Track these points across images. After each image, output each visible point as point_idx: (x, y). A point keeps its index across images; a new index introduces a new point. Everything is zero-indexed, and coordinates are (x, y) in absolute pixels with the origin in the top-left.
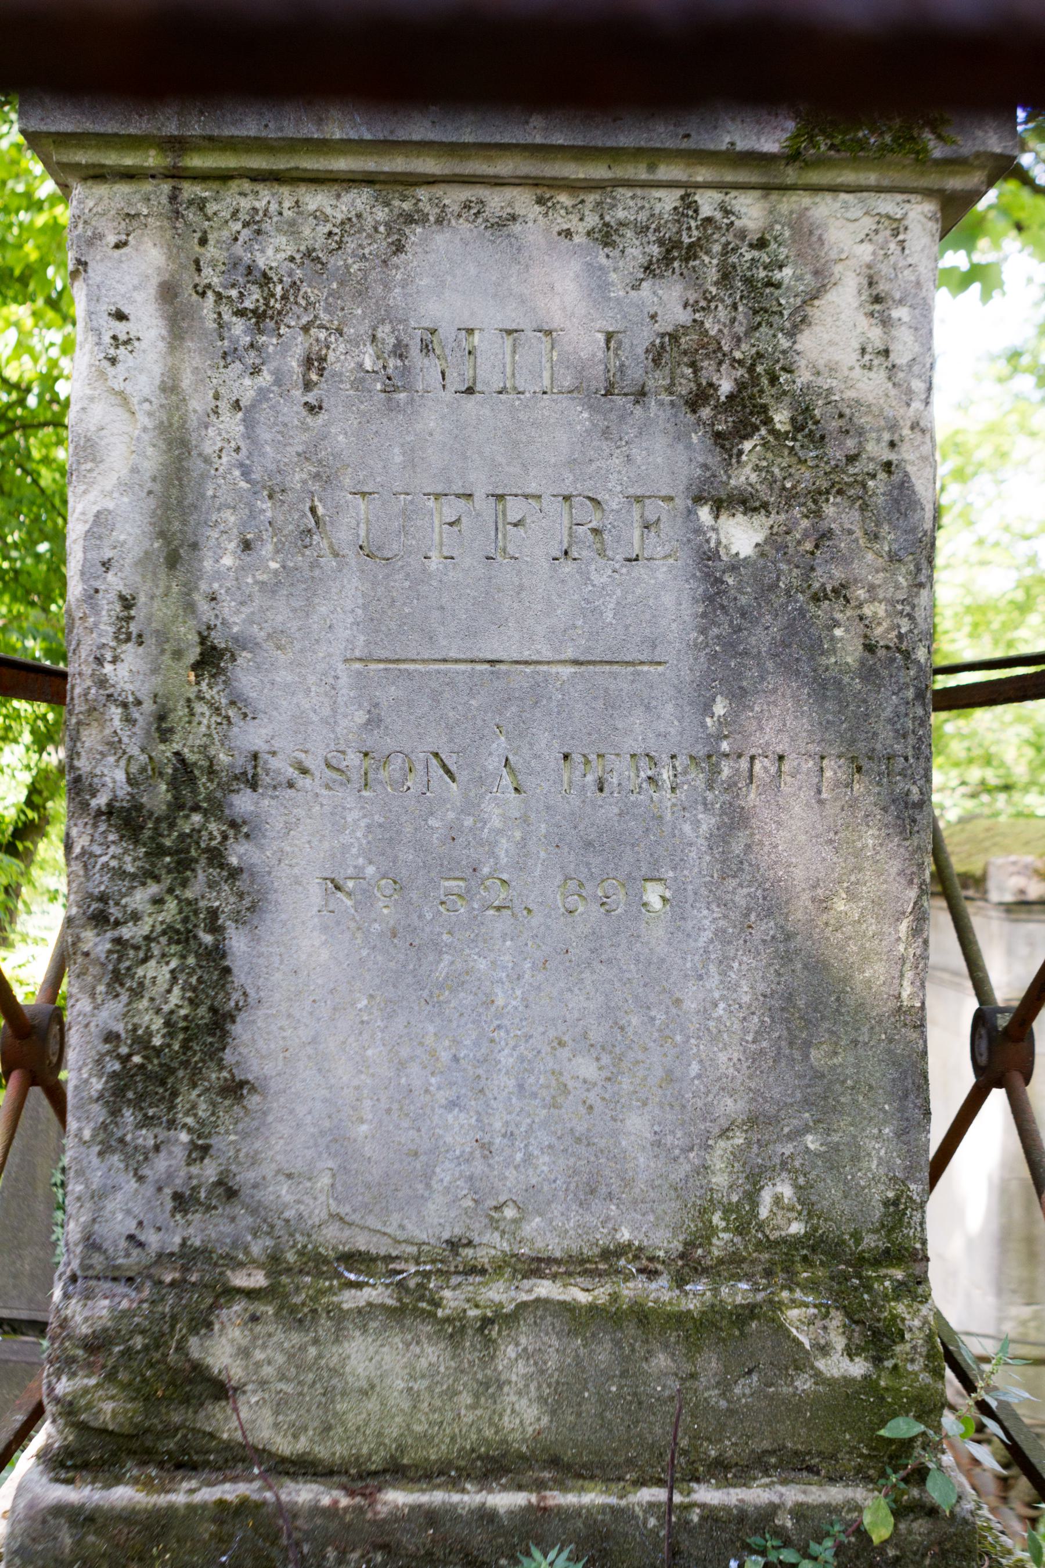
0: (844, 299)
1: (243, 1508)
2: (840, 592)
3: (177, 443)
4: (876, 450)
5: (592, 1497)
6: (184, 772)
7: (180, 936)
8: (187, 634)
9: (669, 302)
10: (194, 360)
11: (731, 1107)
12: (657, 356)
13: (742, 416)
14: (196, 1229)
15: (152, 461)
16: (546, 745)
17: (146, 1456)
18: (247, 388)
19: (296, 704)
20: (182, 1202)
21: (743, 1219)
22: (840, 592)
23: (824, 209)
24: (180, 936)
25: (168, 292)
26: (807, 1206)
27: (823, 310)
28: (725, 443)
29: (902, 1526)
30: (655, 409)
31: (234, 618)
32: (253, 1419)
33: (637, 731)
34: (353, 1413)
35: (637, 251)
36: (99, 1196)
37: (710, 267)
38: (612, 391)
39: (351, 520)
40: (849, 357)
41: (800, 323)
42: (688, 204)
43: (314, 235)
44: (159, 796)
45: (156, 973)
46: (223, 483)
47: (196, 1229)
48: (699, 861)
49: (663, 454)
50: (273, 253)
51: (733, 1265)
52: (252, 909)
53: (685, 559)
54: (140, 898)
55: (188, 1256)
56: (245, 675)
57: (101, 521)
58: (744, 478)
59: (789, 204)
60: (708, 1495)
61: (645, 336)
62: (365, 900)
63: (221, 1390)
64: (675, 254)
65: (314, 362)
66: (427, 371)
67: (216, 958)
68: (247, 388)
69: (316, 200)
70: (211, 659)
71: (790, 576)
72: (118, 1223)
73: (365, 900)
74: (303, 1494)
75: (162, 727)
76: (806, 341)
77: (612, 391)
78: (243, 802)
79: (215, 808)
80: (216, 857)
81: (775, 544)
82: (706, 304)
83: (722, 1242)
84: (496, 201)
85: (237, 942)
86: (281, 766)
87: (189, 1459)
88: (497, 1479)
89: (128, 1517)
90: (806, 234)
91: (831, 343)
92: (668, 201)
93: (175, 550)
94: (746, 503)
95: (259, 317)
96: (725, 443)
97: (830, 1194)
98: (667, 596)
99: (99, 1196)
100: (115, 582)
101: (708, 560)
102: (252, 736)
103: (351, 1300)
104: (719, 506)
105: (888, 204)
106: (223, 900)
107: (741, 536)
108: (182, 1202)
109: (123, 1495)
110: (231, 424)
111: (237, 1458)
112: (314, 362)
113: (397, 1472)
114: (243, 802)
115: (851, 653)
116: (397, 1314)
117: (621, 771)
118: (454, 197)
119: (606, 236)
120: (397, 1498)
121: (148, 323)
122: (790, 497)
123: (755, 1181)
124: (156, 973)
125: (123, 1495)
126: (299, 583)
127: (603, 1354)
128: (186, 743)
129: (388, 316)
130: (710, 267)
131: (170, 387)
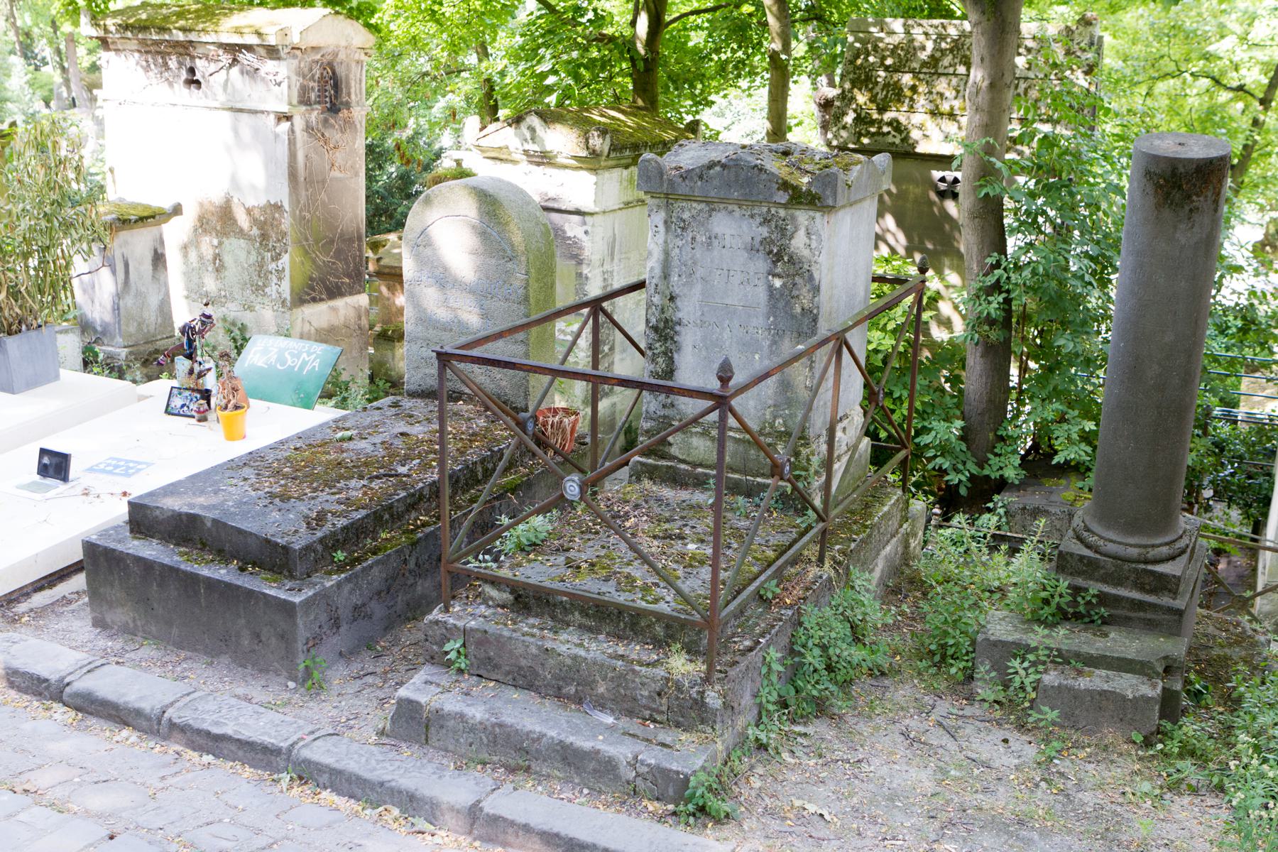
0: (801, 233)
1: (671, 467)
2: (797, 297)
3: (667, 253)
4: (806, 267)
5: (736, 476)
6: (666, 321)
7: (665, 353)
8: (668, 293)
9: (764, 231)
10: (670, 237)
11: (770, 402)
12: (761, 243)
13: (778, 257)
14: (666, 412)
15: (662, 257)
16: (736, 323)
17: (656, 455)
18: (680, 243)
19: (687, 310)
20: (664, 406)
21: (772, 426)
22: (797, 297)
23: (798, 213)
24: (665, 353)
25: (666, 222)
26: (785, 425)
27: (796, 235)
28: (775, 263)
29: (920, 110)
30: (761, 254)
31: (677, 291)
32: (674, 451)
33: (754, 322)
34: (694, 452)
35: (759, 220)
36: (649, 403)
37: (773, 224)
38: (752, 249)
39: (700, 272)
40: (802, 246)
41: (791, 238)
42: (769, 210)
43: (694, 212)
44: (661, 325)
45: (660, 360)
46: (675, 262)
47: (666, 412)
48: (766, 350)
49: (762, 264)
50: (686, 216)
51: (769, 434)
52: (678, 350)
53: (765, 287)
54: (657, 345)
55: (665, 417)
56: (678, 302)
57: (652, 268)
58: (779, 270)
59: (790, 212)
60: (759, 480)
61: (758, 239)
62: (700, 350)
63: (670, 444)
64: (766, 221)
65: (693, 238)
66: (715, 243)
67: (671, 358)
68: (680, 243)
69: (695, 205)
70: (672, 299)
71: (787, 292)
72: (652, 409)
73: (700, 350)
74: (683, 466)
75: (663, 311)
76: (793, 242)
77: (752, 249)
78: (678, 328)
79: (672, 329)
80: (672, 338)
81: (784, 285)
82: (772, 232)
83: (768, 430)
84: (730, 207)
85: (676, 356)
86: (685, 321)
87: (663, 456)
88: (177, 544)
89: (651, 465)
90: (793, 218)
91: (799, 243)
92: (765, 209)
93: (666, 276)
94: (779, 276)
95: (683, 229)
96: (775, 263)
97: (790, 423)
98: (761, 295)
99: (649, 403)
100: (654, 281)
101: (771, 287)
102: (680, 315)
103: (694, 430)
104: (774, 276)
105: (811, 213)
106: (673, 347)
107: (778, 283)
108: (664, 406)
109: (650, 461)
110: (677, 251)
111: (673, 458)
112: (693, 238)
113: (701, 465)
114: (678, 328)
115: (798, 310)
116: (702, 434)
117: (751, 330)
118: (722, 206)
119: (752, 216)
120: (700, 470)
121: (662, 228)
122: (788, 276)
123: (775, 418)
124: (660, 360)
125: (650, 461)
126: (689, 284)
127: (741, 449)
128: (667, 315)
129: (708, 230)
130: (773, 224)
131: (666, 242)
